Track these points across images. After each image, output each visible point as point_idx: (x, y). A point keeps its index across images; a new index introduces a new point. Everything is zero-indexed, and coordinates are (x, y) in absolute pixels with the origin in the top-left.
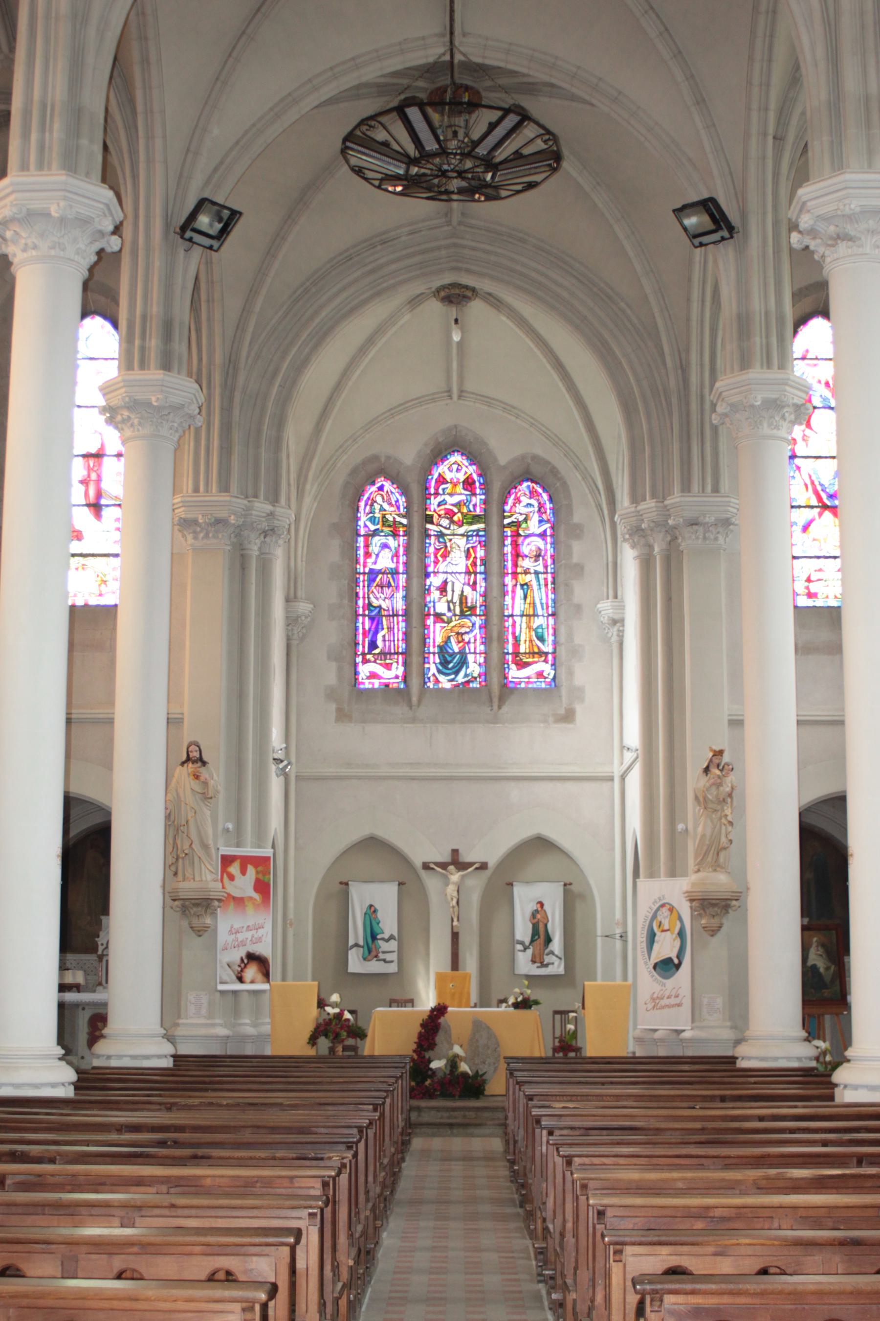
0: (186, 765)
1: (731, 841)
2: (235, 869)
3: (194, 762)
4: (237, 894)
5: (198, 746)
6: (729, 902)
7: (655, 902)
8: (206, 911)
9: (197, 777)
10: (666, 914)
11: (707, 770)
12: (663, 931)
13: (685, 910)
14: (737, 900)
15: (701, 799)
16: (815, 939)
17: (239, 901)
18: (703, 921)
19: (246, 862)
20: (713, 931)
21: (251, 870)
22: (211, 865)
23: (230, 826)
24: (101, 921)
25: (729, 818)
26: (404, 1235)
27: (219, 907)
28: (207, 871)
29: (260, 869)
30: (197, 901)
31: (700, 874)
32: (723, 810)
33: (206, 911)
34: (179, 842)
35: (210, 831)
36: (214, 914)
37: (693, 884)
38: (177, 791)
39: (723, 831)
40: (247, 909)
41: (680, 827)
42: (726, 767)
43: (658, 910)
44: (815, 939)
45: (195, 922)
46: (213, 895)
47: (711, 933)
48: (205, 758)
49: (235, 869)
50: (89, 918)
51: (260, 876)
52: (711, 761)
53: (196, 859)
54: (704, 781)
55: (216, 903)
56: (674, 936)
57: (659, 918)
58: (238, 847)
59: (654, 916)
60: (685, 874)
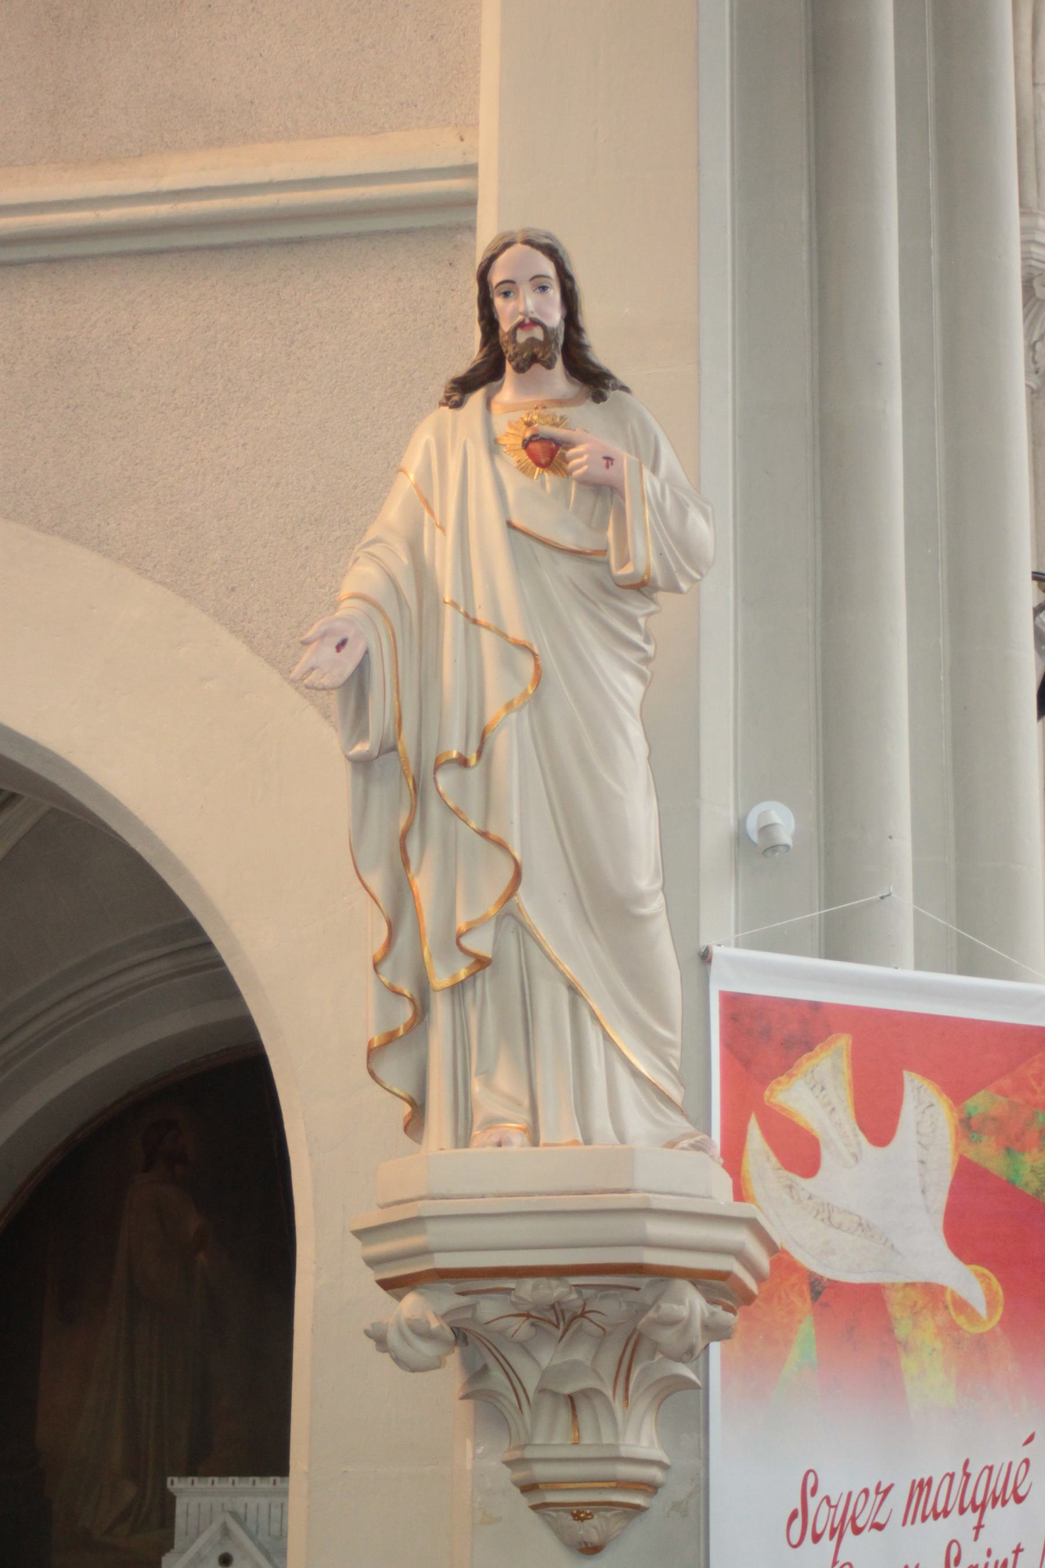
0: (477, 398)
2: (816, 1093)
3: (532, 359)
4: (843, 1263)
5: (552, 252)
8: (624, 1371)
9: (547, 452)
17: (856, 1312)
19: (886, 1053)
21: (925, 1112)
22: (655, 1045)
23: (784, 821)
24: (167, 1504)
26: (517, 1454)
27: (715, 1331)
28: (625, 1082)
29: (980, 1103)
30: (555, 1290)
33: (624, 1371)
34: (424, 883)
35: (641, 812)
36: (684, 1404)
38: (414, 547)
40: (909, 1364)
45: (551, 1439)
46: (664, 1242)
48: (602, 348)
49: (816, 1093)
50: (130, 1491)
51: (987, 1154)
53: (551, 1001)
55: (692, 1304)
58: (832, 949)
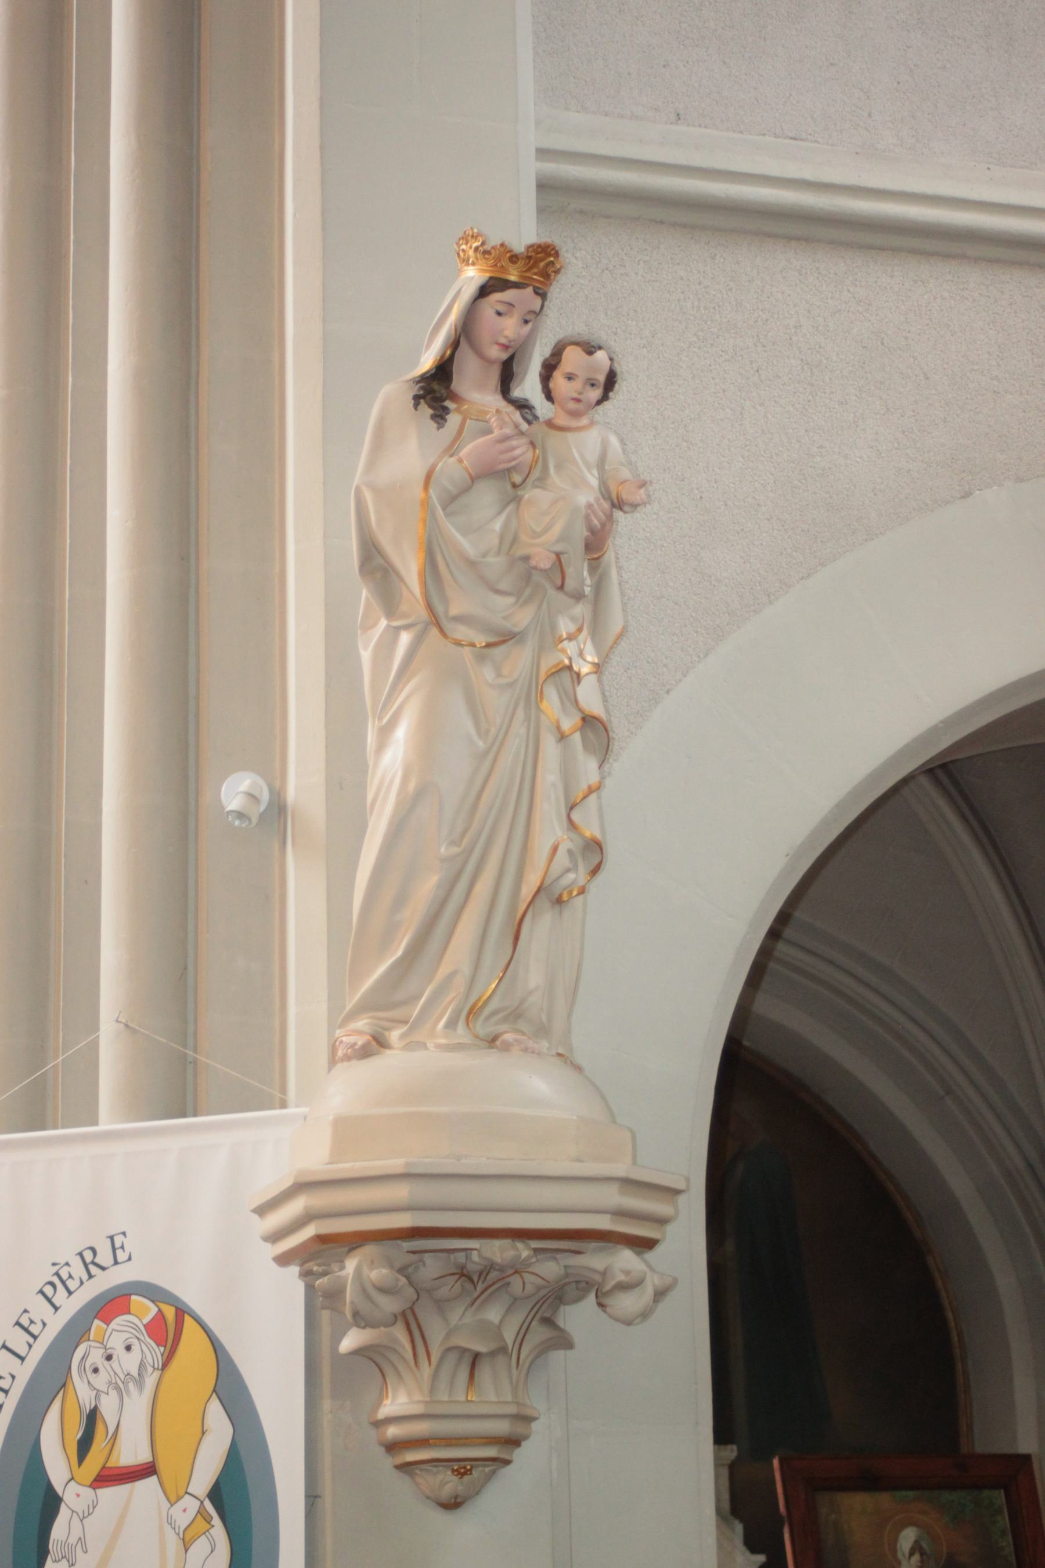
1: (594, 853)
6: (594, 1260)
7: (60, 1280)
10: (130, 1363)
11: (436, 389)
12: (109, 1477)
13: (268, 1329)
14: (644, 1245)
15: (409, 567)
16: (908, 1537)
18: (397, 1402)
20: (462, 1468)
25: (589, 697)
31: (393, 1064)
32: (551, 639)
37: (347, 1131)
39: (549, 776)
41: (236, 791)
42: (573, 358)
43: (75, 1332)
44: (908, 1537)
47: (449, 1484)
52: (465, 334)
54: (414, 449)
56: (186, 1510)
57: (82, 1392)
59: (51, 1379)
60: (261, 1088)
